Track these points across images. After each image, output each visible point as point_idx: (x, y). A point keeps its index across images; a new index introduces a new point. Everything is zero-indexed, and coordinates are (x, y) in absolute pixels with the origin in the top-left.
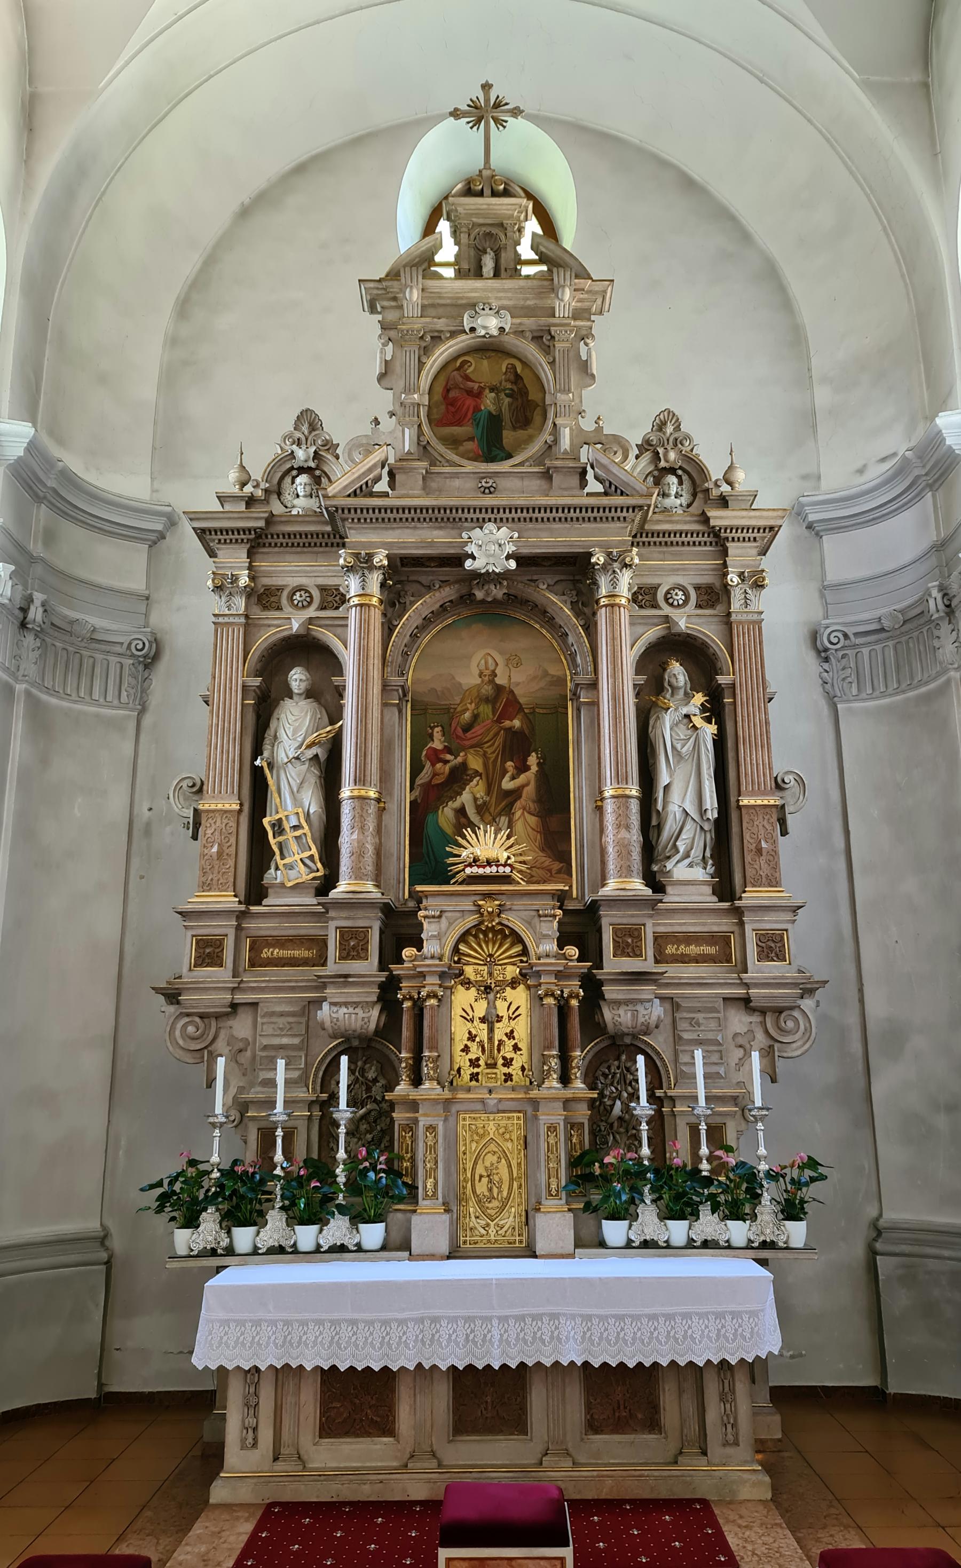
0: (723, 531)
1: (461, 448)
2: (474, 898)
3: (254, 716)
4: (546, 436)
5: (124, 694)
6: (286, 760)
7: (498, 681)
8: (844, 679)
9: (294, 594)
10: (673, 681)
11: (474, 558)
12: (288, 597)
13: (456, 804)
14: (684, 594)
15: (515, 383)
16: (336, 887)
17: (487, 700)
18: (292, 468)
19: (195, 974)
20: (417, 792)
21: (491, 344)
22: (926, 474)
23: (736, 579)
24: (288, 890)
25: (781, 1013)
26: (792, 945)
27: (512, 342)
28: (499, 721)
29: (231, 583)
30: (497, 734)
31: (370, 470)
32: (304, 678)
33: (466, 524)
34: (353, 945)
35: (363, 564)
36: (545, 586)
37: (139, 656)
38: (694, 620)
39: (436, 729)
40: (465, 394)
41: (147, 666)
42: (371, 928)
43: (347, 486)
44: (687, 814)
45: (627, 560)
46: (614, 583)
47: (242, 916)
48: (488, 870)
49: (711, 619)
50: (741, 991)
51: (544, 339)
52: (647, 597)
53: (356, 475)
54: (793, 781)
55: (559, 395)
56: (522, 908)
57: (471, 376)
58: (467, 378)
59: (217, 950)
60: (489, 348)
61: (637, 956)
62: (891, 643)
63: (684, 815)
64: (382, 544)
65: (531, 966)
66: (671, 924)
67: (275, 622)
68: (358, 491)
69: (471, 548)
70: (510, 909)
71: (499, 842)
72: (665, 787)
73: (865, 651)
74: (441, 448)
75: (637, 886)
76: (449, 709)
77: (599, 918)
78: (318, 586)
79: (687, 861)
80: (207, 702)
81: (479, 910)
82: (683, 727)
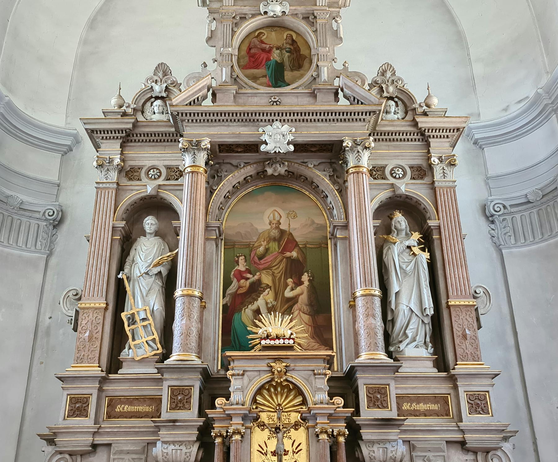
0: (426, 131)
1: (258, 81)
2: (267, 361)
3: (120, 249)
4: (312, 72)
5: (39, 243)
6: (139, 275)
7: (282, 227)
8: (505, 234)
9: (149, 171)
10: (398, 226)
11: (267, 144)
12: (145, 173)
13: (254, 307)
14: (403, 171)
15: (292, 45)
16: (169, 358)
17: (274, 239)
18: (152, 97)
19: (66, 422)
20: (227, 299)
21: (277, 22)
22: (552, 103)
23: (437, 161)
24: (137, 363)
25: (488, 452)
26: (494, 402)
27: (291, 21)
28: (282, 252)
29: (109, 163)
30: (281, 261)
31: (200, 90)
32: (154, 223)
33: (261, 124)
34: (180, 399)
35: (196, 146)
36: (312, 166)
37: (50, 220)
38: (411, 186)
39: (241, 258)
40: (261, 51)
41: (55, 227)
42: (193, 386)
43: (185, 99)
44: (412, 311)
45: (367, 145)
46: (359, 159)
47: (103, 381)
48: (277, 342)
49: (421, 186)
50: (458, 436)
51: (310, 18)
52: (379, 173)
53: (191, 93)
54: (482, 293)
55: (320, 48)
56: (301, 368)
57: (265, 41)
58: (262, 42)
59: (84, 405)
60: (276, 25)
61: (384, 407)
62: (535, 210)
63: (410, 312)
64: (207, 135)
65: (309, 410)
66: (406, 388)
67: (136, 188)
68: (192, 103)
69: (264, 138)
70: (293, 370)
71: (285, 324)
72: (396, 293)
73: (518, 216)
74: (246, 80)
75: (382, 356)
76: (249, 245)
77: (356, 380)
78: (165, 166)
79: (414, 344)
80: (88, 241)
81: (271, 370)
82: (406, 256)
